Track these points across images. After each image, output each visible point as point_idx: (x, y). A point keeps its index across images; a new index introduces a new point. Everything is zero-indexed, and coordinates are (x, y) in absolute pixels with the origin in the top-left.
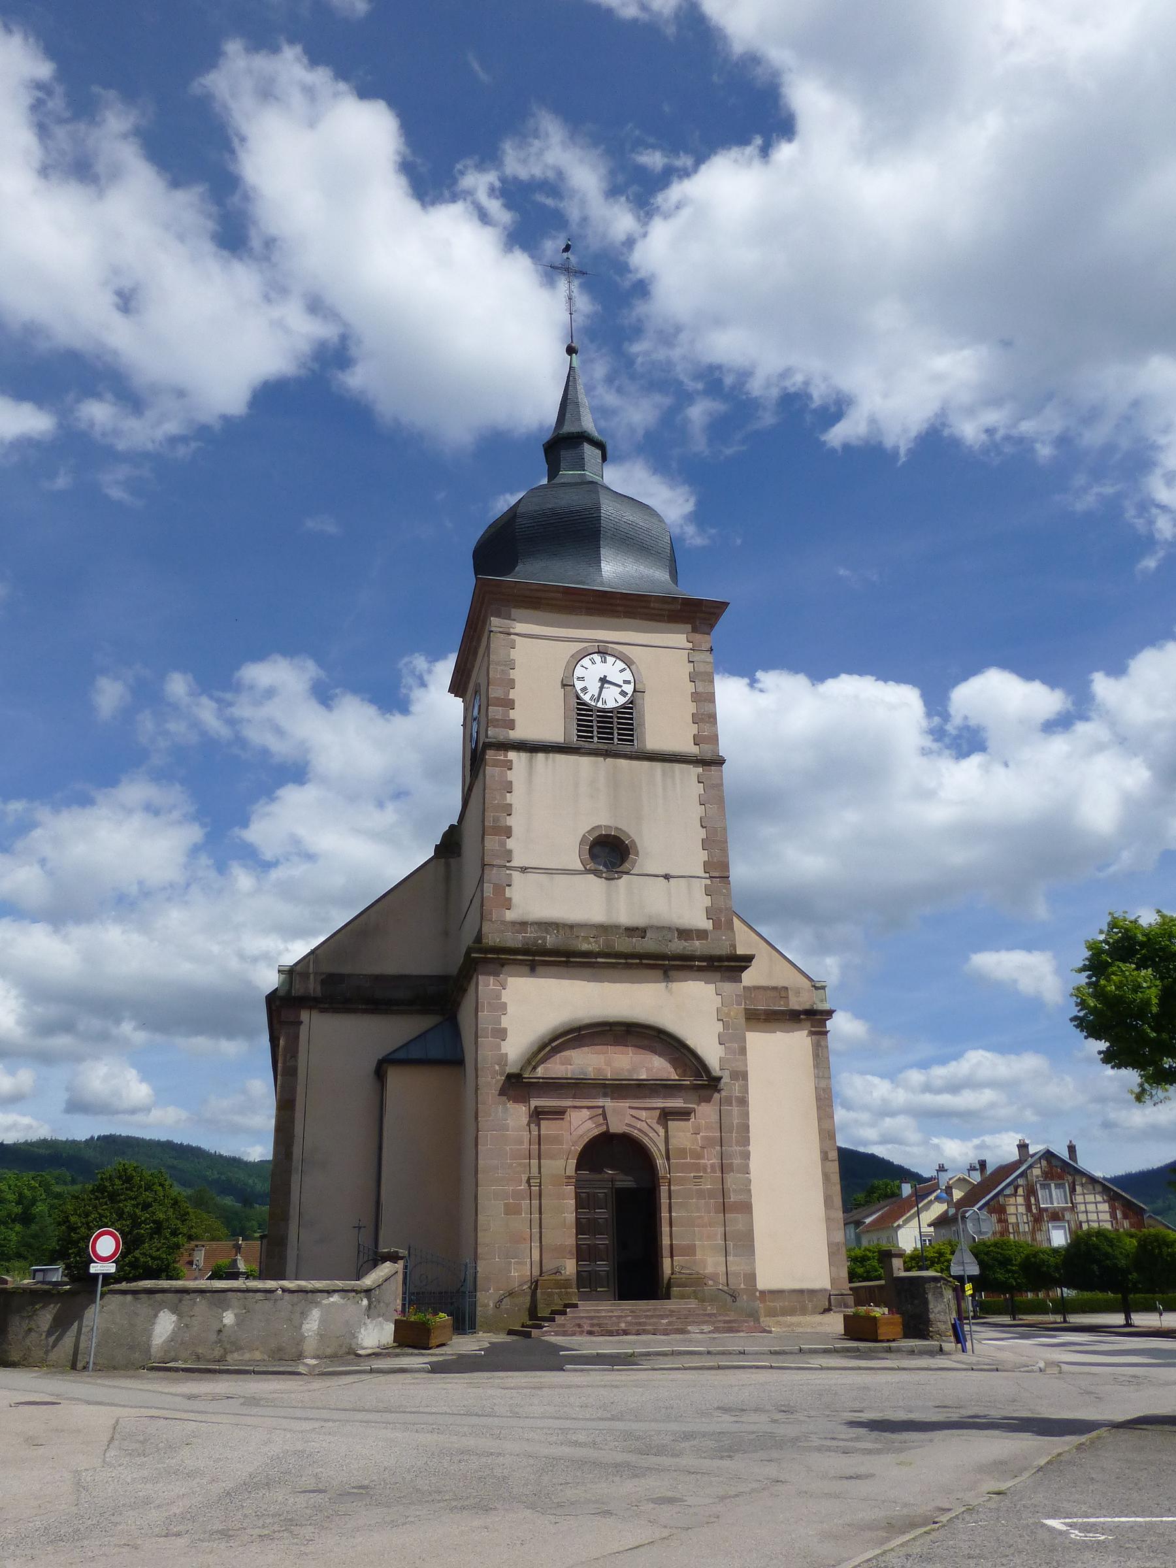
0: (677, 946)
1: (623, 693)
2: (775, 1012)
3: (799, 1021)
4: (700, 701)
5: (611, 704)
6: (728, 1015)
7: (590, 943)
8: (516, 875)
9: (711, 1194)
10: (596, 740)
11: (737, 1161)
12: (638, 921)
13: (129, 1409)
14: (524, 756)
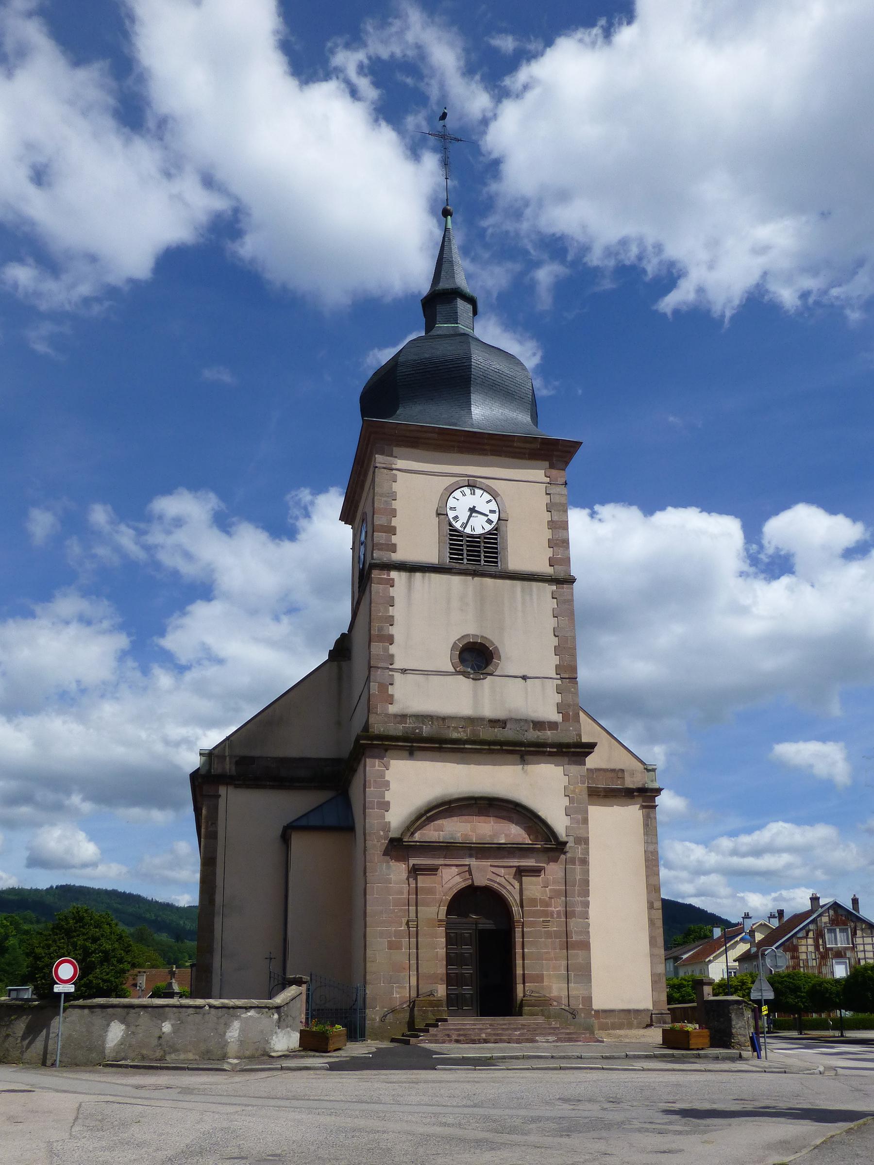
0: (532, 735)
1: (489, 522)
3: (633, 797)
8: (397, 676)
9: (557, 935)
11: (578, 909)
14: (404, 575)
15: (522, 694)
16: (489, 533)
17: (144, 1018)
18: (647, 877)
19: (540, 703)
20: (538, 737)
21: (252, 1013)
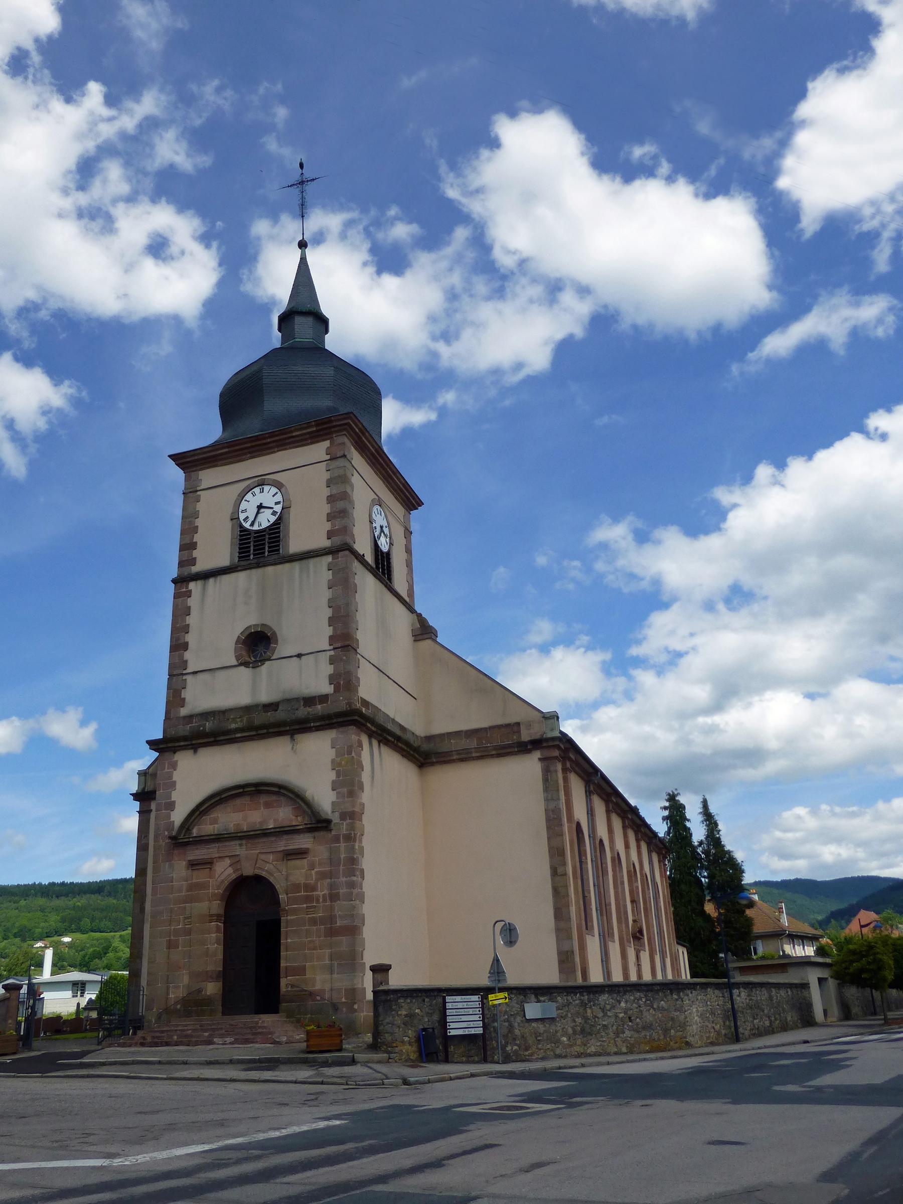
0: (302, 712)
1: (274, 513)
2: (504, 747)
3: (529, 751)
4: (334, 501)
5: (265, 525)
6: (340, 764)
7: (236, 723)
8: (189, 678)
10: (252, 557)
11: (343, 891)
13: (337, 1086)
14: (199, 583)
15: (301, 673)
16: (274, 524)
18: (549, 839)
19: (313, 679)
20: (308, 713)
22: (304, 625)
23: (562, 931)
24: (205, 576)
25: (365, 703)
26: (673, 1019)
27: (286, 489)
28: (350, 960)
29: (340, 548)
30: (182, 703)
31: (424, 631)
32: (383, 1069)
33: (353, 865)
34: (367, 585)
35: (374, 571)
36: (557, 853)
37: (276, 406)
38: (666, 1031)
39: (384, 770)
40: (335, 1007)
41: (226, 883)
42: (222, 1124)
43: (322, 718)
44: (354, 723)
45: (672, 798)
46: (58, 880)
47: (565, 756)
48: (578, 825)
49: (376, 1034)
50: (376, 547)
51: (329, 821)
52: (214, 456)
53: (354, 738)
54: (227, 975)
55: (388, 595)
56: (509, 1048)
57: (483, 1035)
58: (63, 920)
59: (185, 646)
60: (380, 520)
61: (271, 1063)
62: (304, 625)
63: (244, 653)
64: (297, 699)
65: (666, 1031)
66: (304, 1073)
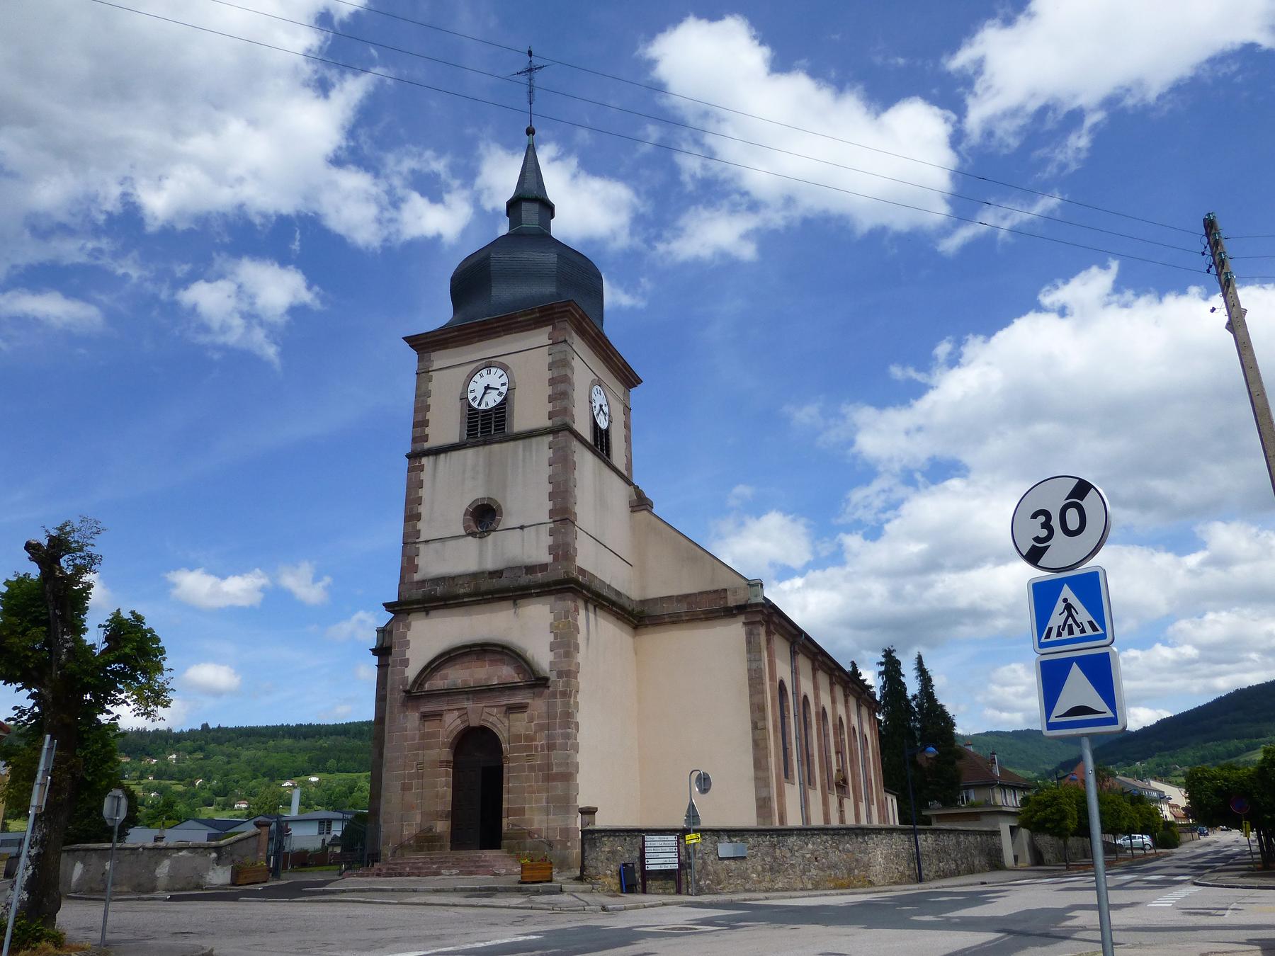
0: (525, 579)
1: (500, 394)
2: (712, 612)
3: (734, 616)
5: (492, 405)
6: (557, 627)
8: (422, 547)
9: (540, 768)
11: (559, 741)
12: (498, 565)
14: (431, 458)
17: (94, 859)
21: (184, 853)
22: (526, 500)
23: (761, 779)
24: (436, 452)
25: (582, 571)
26: (857, 860)
27: (511, 372)
28: (564, 802)
29: (561, 429)
30: (415, 568)
31: (640, 503)
32: (587, 898)
33: (568, 719)
34: (586, 462)
35: (592, 449)
36: (758, 709)
37: (503, 293)
38: (850, 871)
39: (599, 635)
40: (550, 845)
41: (455, 733)
42: (438, 938)
43: (541, 586)
44: (569, 590)
45: (888, 654)
46: (305, 722)
47: (769, 619)
48: (782, 683)
49: (583, 868)
50: (595, 424)
51: (547, 679)
52: (445, 339)
53: (570, 604)
54: (456, 814)
55: (607, 472)
56: (702, 883)
57: (679, 870)
58: (310, 760)
59: (418, 517)
60: (599, 399)
61: (490, 892)
62: (526, 500)
63: (472, 524)
64: (519, 568)
65: (850, 871)
66: (517, 900)
